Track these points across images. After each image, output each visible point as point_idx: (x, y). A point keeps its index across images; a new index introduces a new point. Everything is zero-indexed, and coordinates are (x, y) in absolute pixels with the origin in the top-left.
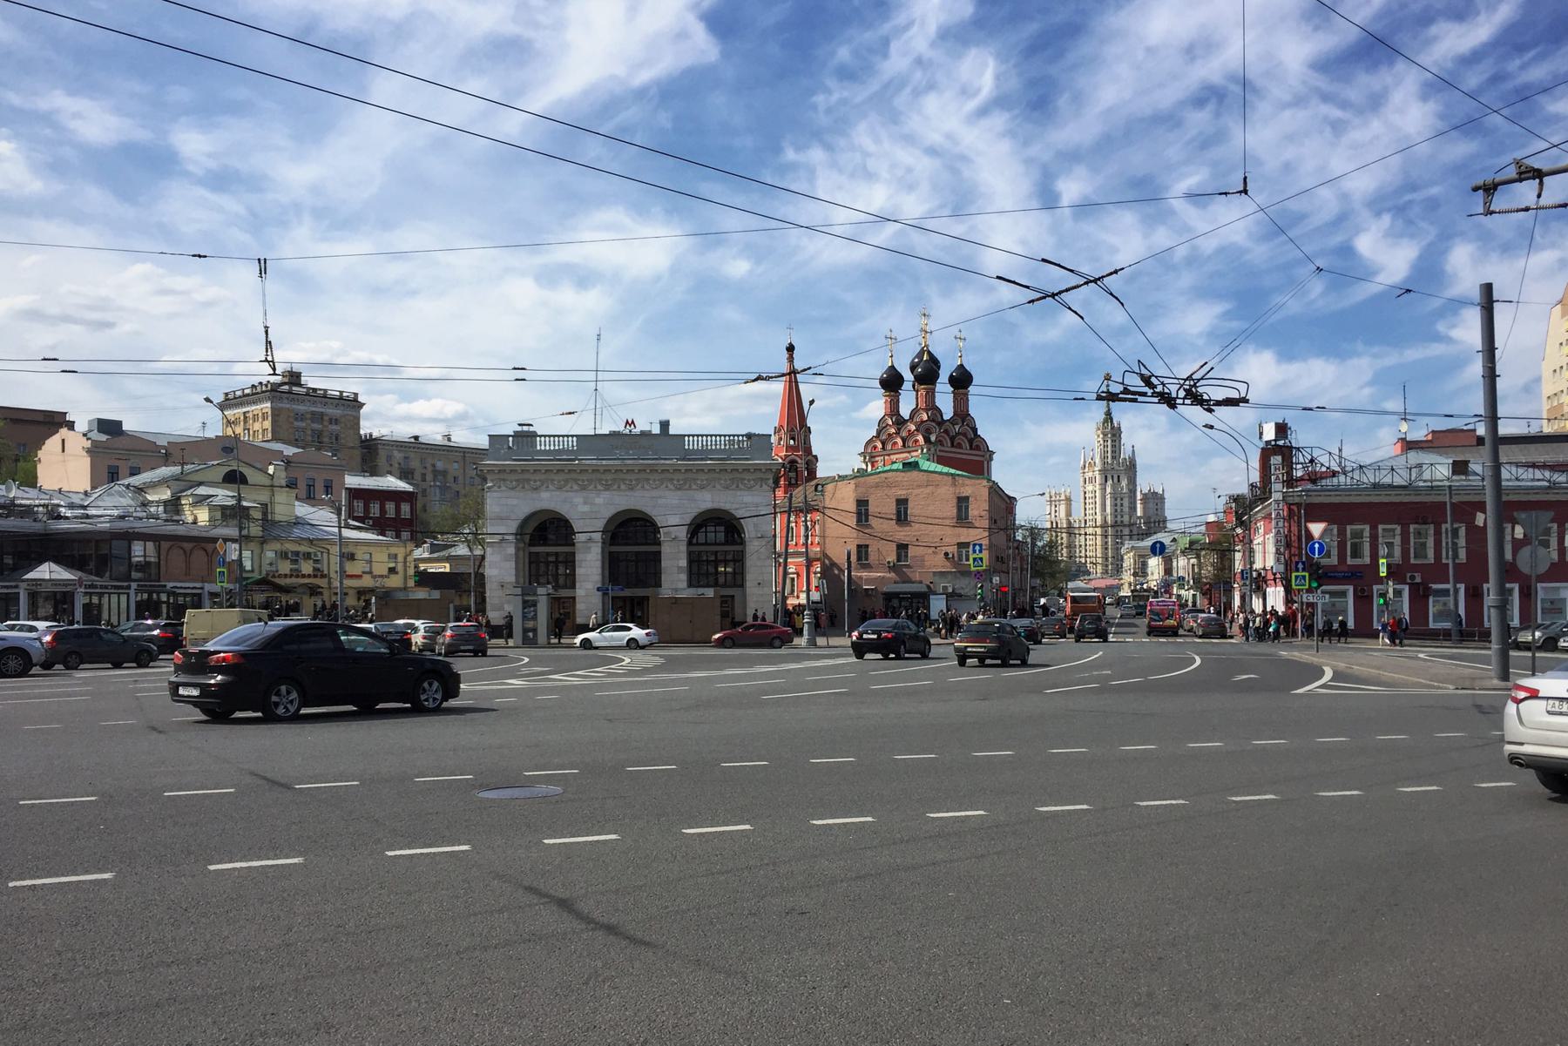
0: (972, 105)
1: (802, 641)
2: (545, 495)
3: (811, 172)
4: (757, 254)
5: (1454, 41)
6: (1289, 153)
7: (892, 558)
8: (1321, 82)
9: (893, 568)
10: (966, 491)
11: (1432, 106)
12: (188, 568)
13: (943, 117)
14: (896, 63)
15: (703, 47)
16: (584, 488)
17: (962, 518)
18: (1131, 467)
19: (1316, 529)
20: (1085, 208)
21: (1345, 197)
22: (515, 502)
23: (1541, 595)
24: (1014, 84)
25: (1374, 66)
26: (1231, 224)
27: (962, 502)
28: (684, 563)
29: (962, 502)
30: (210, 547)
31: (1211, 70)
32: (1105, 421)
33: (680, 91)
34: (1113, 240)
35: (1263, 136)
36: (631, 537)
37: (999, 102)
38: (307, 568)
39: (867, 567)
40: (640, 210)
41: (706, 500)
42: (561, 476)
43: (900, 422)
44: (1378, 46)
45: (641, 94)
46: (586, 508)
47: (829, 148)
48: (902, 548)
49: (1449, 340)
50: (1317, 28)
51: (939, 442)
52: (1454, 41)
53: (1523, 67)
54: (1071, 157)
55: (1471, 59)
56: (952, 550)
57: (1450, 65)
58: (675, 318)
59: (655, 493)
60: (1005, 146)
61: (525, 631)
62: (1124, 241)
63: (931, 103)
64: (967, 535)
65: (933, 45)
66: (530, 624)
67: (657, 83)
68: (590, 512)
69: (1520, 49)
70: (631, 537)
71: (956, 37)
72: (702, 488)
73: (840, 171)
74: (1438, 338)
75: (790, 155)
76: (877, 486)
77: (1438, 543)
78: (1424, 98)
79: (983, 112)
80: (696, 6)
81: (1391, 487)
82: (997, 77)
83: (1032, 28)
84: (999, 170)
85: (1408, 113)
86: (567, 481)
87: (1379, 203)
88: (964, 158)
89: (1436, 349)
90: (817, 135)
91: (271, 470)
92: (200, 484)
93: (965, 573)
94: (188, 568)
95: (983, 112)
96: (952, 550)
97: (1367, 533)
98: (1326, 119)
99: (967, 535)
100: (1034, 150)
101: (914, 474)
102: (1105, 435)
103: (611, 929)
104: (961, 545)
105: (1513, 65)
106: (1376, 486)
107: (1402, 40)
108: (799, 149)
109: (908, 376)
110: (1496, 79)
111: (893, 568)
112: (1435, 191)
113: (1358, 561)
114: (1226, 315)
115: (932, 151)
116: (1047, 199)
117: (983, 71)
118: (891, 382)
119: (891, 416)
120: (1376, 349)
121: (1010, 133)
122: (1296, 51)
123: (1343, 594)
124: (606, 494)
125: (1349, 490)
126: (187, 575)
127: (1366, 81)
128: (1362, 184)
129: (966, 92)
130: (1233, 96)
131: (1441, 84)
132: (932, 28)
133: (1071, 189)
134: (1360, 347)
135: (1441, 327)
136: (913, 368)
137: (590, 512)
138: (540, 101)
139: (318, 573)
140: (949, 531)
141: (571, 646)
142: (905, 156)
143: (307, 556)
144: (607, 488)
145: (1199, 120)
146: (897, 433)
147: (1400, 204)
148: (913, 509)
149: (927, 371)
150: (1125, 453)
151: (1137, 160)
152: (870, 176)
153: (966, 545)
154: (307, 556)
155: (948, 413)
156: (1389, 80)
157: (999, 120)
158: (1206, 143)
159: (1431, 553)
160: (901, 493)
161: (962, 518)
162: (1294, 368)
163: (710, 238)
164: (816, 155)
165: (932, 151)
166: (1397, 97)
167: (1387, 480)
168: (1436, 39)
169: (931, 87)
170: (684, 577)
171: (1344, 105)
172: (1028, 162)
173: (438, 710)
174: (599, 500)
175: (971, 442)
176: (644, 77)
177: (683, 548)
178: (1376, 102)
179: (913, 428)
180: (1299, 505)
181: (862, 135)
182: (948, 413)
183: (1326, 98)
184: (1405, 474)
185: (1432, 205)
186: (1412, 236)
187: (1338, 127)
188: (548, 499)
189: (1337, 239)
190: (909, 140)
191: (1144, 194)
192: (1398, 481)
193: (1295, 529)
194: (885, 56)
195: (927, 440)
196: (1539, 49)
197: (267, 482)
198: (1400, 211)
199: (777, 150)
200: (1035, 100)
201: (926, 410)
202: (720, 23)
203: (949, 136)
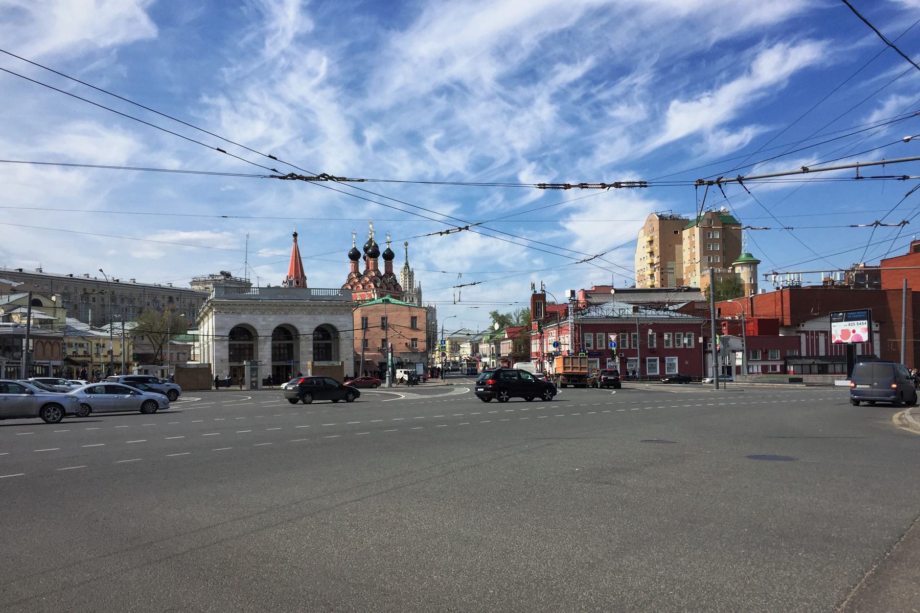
0: (315, 81)
1: (386, 385)
2: (243, 316)
3: (219, 109)
4: (183, 155)
6: (484, 126)
7: (380, 346)
8: (500, 89)
9: (380, 351)
10: (415, 314)
11: (555, 107)
12: (44, 353)
13: (298, 87)
14: (270, 51)
15: (146, 29)
16: (263, 313)
17: (413, 327)
18: (419, 293)
20: (379, 146)
21: (513, 151)
22: (228, 319)
23: (667, 361)
24: (336, 72)
25: (527, 84)
26: (455, 162)
27: (414, 319)
28: (311, 349)
29: (414, 319)
30: (61, 342)
31: (442, 77)
32: (405, 268)
33: (128, 53)
34: (396, 165)
35: (473, 116)
36: (285, 336)
37: (330, 81)
38: (81, 352)
39: (368, 350)
40: (108, 125)
41: (322, 319)
42: (252, 307)
43: (359, 276)
45: (107, 51)
46: (264, 323)
47: (231, 99)
48: (384, 341)
49: (564, 229)
51: (381, 287)
53: (599, 92)
54: (376, 116)
55: (575, 84)
56: (409, 342)
57: (564, 86)
58: (134, 195)
59: (297, 316)
60: (334, 107)
61: (252, 382)
62: (404, 166)
63: (293, 78)
64: (415, 335)
65: (292, 43)
66: (254, 379)
67: (113, 46)
68: (264, 325)
69: (596, 83)
70: (285, 336)
71: (304, 41)
72: (320, 314)
73: (236, 111)
75: (205, 99)
76: (372, 311)
77: (630, 341)
78: (552, 103)
79: (321, 87)
80: (143, 3)
82: (329, 67)
83: (346, 43)
84: (331, 120)
85: (544, 111)
86: (254, 310)
87: (531, 157)
88: (309, 111)
89: (557, 234)
90: (224, 90)
91: (54, 298)
92: (20, 306)
93: (415, 352)
94: (44, 353)
95: (321, 87)
96: (409, 342)
99: (415, 335)
100: (352, 110)
101: (388, 306)
102: (405, 275)
104: (413, 340)
105: (594, 90)
106: (607, 317)
107: (541, 70)
108: (211, 97)
109: (362, 253)
110: (586, 97)
111: (380, 351)
112: (557, 151)
114: (457, 211)
115: (292, 106)
116: (358, 137)
117: (320, 62)
118: (354, 256)
119: (355, 273)
121: (338, 100)
122: (489, 71)
123: (656, 360)
124: (274, 316)
126: (44, 356)
127: (522, 92)
128: (521, 145)
129: (311, 74)
130: (454, 91)
131: (558, 97)
132: (290, 35)
133: (372, 135)
134: (522, 230)
135: (561, 223)
136: (366, 249)
137: (264, 325)
138: (35, 51)
139: (86, 354)
140: (407, 331)
141: (280, 389)
142: (276, 107)
143: (81, 346)
144: (275, 313)
145: (441, 103)
146: (359, 282)
148: (390, 321)
149: (372, 252)
150: (416, 285)
151: (407, 122)
152: (253, 117)
153: (416, 339)
154: (81, 346)
155: (383, 272)
156: (535, 92)
157: (330, 92)
158: (445, 116)
159: (604, 344)
160: (383, 314)
161: (413, 327)
162: (489, 240)
163: (158, 147)
164: (222, 101)
165: (292, 106)
166: (539, 101)
167: (611, 315)
168: (557, 73)
169: (290, 68)
170: (311, 356)
171: (512, 102)
172: (348, 117)
174: (271, 319)
175: (395, 287)
176: (108, 42)
177: (311, 342)
178: (528, 103)
179: (368, 279)
181: (252, 93)
182: (383, 272)
183: (504, 98)
185: (556, 159)
186: (546, 174)
187: (511, 114)
188: (244, 319)
189: (509, 173)
190: (279, 97)
191: (413, 139)
192: (615, 315)
194: (263, 46)
195: (376, 286)
196: (605, 83)
197: (52, 305)
198: (540, 160)
199: (198, 96)
200: (353, 82)
201: (374, 271)
202: (160, 14)
203: (303, 98)
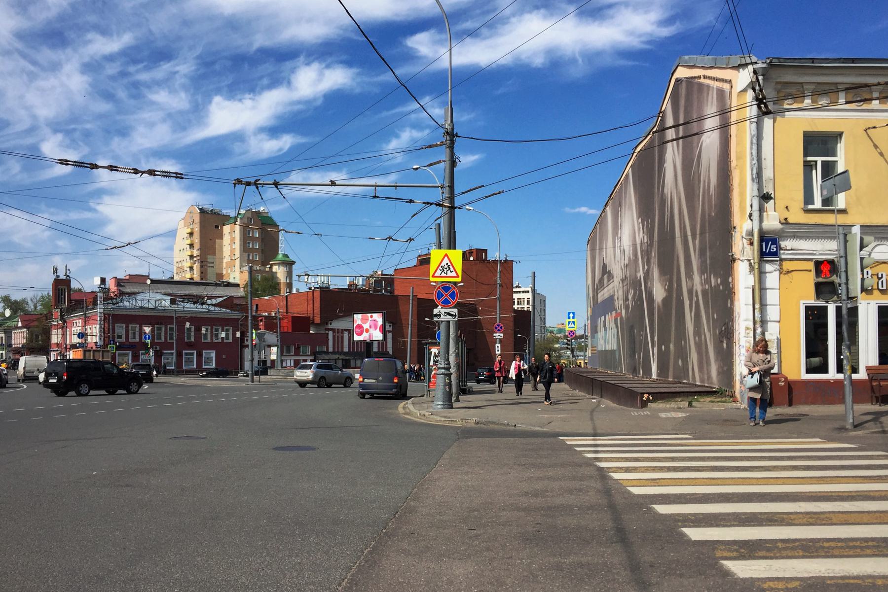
5: (103, 46)
8: (19, 45)
11: (85, 78)
19: (147, 329)
21: (34, 117)
23: (204, 355)
25: (53, 47)
44: (56, 35)
49: (95, 211)
50: (18, 14)
52: (103, 46)
53: (138, 71)
55: (110, 58)
69: (135, 62)
74: (90, 210)
77: (166, 333)
81: (148, 308)
87: (56, 127)
89: (88, 215)
97: (137, 329)
98: (23, 71)
103: (188, 437)
105: (132, 69)
106: (142, 308)
112: (88, 126)
113: (134, 340)
120: (52, 210)
125: (131, 309)
128: (45, 111)
131: (91, 67)
134: (43, 206)
135: (92, 204)
147: (66, 126)
156: (63, 57)
159: (163, 338)
166: (68, 68)
167: (146, 306)
171: (34, 63)
173: (136, 393)
178: (54, 67)
180: (109, 315)
183: (24, 56)
184: (153, 303)
185: (87, 134)
186: (75, 149)
187: (32, 77)
189: (29, 141)
192: (151, 306)
193: (107, 325)
